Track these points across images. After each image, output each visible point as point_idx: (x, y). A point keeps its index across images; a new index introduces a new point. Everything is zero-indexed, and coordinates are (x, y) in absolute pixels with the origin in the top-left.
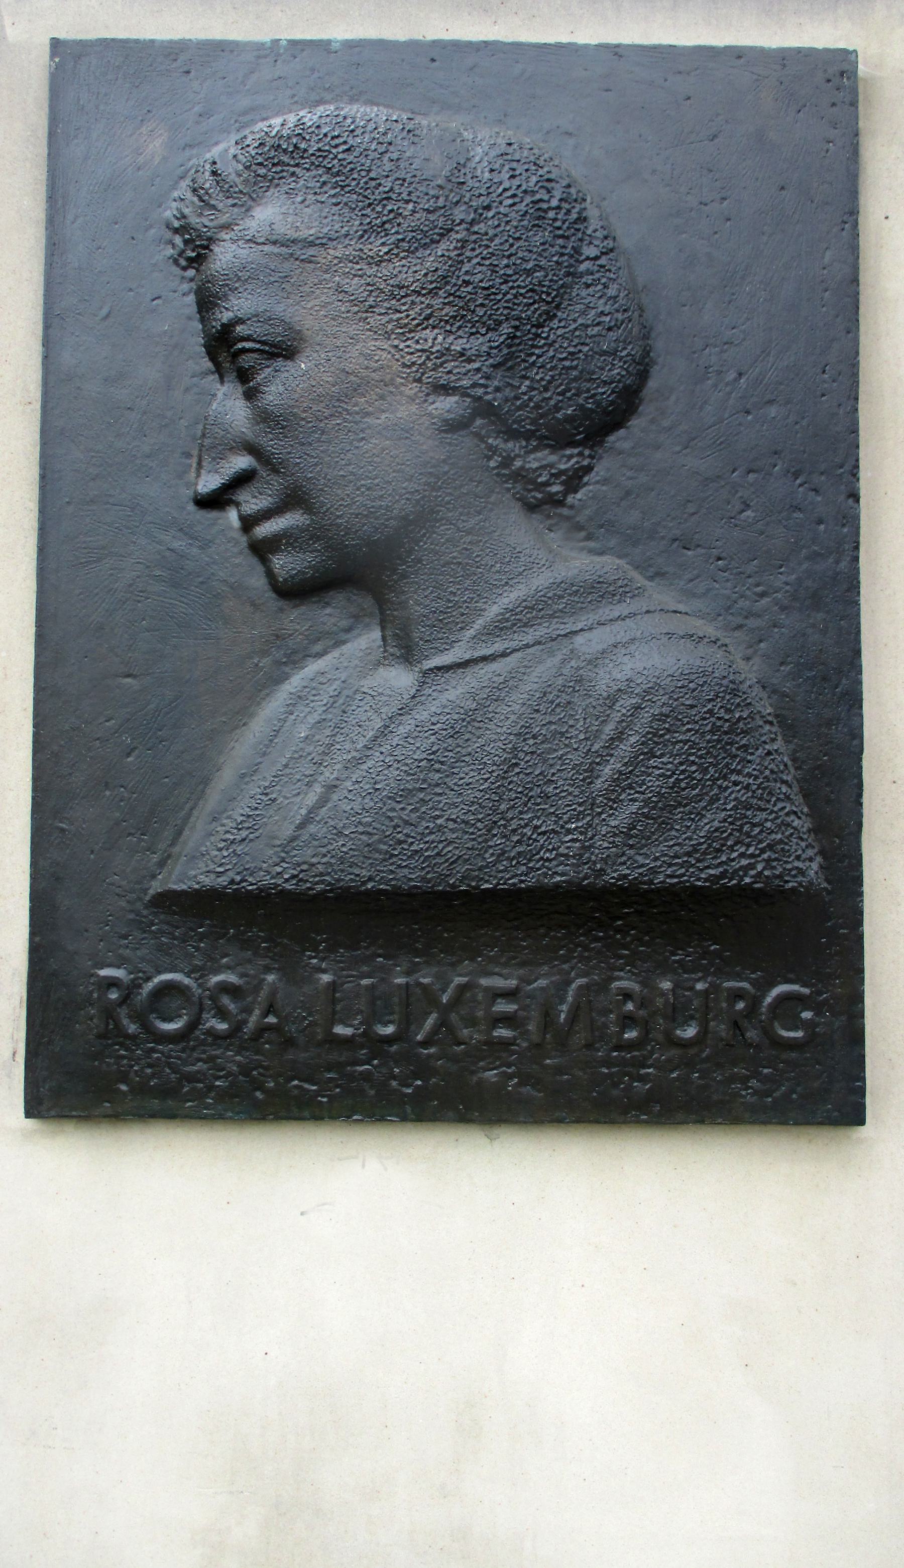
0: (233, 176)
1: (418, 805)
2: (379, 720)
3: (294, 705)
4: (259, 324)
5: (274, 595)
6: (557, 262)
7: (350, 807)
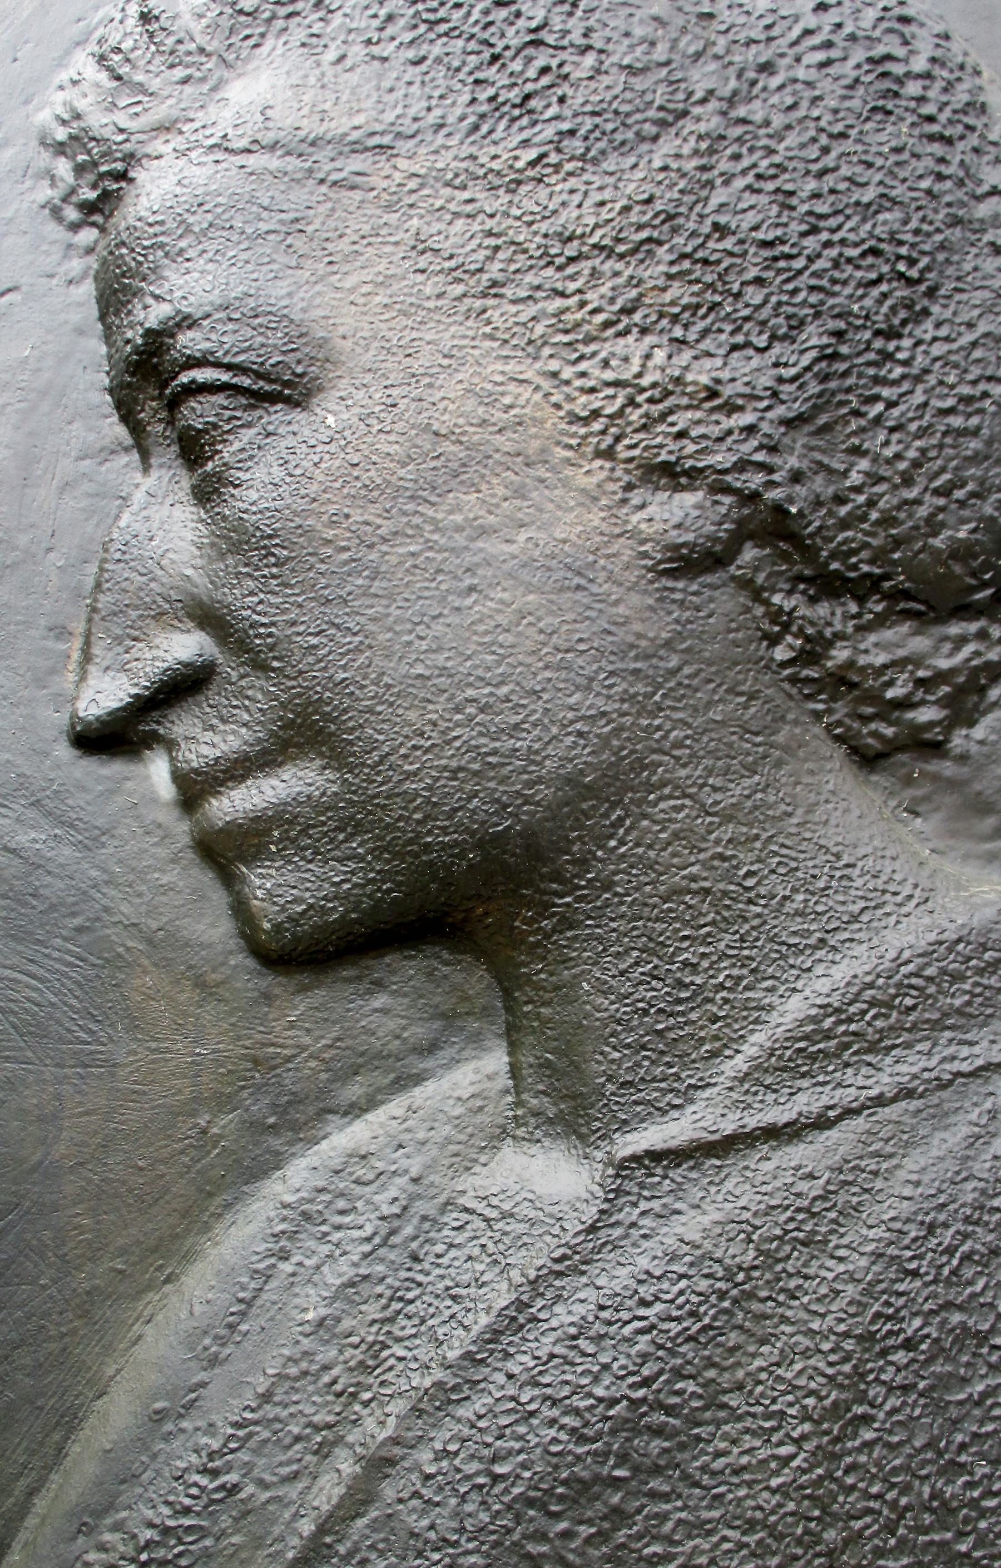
0: (187, 21)
1: (606, 1525)
2: (504, 1286)
3: (292, 1236)
4: (230, 326)
5: (251, 963)
6: (929, 192)
7: (425, 1523)
